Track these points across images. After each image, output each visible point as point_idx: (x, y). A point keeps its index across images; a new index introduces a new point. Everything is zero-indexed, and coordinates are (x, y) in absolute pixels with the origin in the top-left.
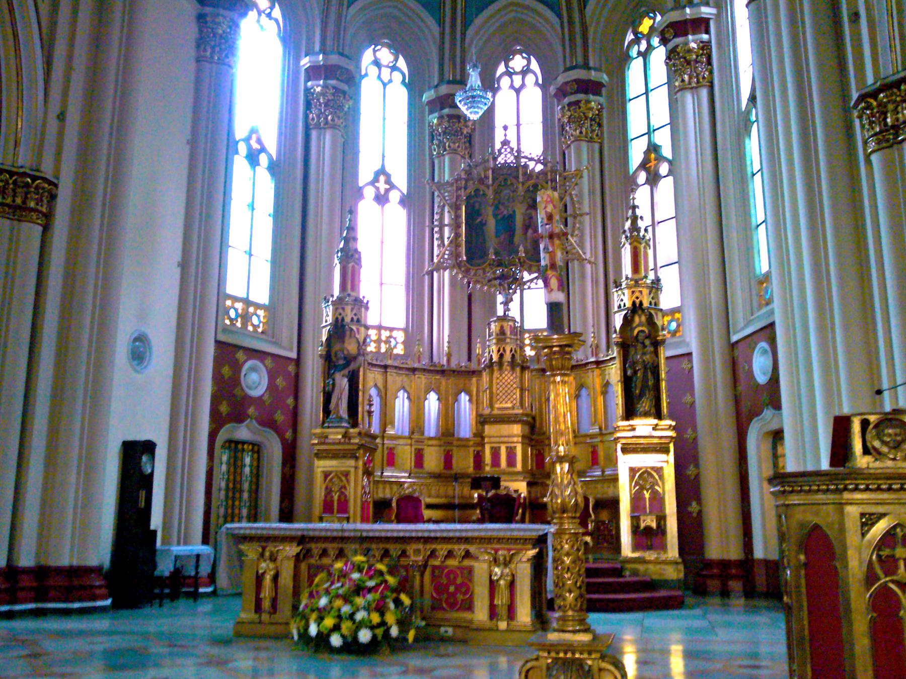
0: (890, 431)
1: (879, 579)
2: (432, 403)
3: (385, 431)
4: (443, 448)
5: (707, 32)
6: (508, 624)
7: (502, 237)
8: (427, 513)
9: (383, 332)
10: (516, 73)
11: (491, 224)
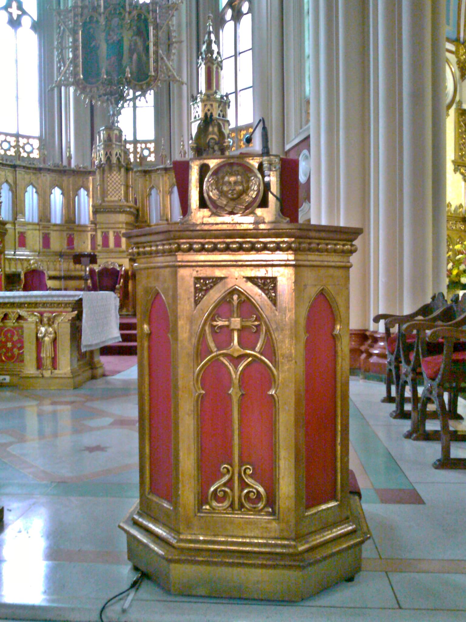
0: (232, 179)
1: (211, 352)
3: (16, 219)
4: (65, 234)
6: (51, 373)
7: (113, 59)
8: (50, 283)
9: (20, 139)
11: (104, 47)
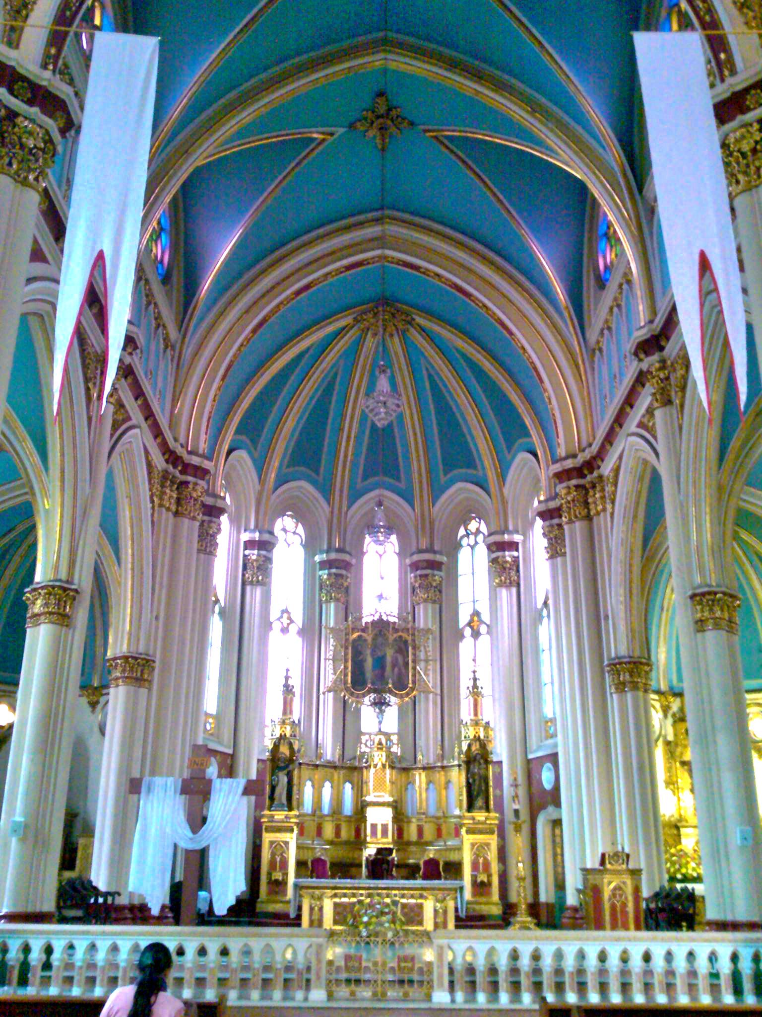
2: (327, 791)
5: (517, 550)
10: (472, 533)
